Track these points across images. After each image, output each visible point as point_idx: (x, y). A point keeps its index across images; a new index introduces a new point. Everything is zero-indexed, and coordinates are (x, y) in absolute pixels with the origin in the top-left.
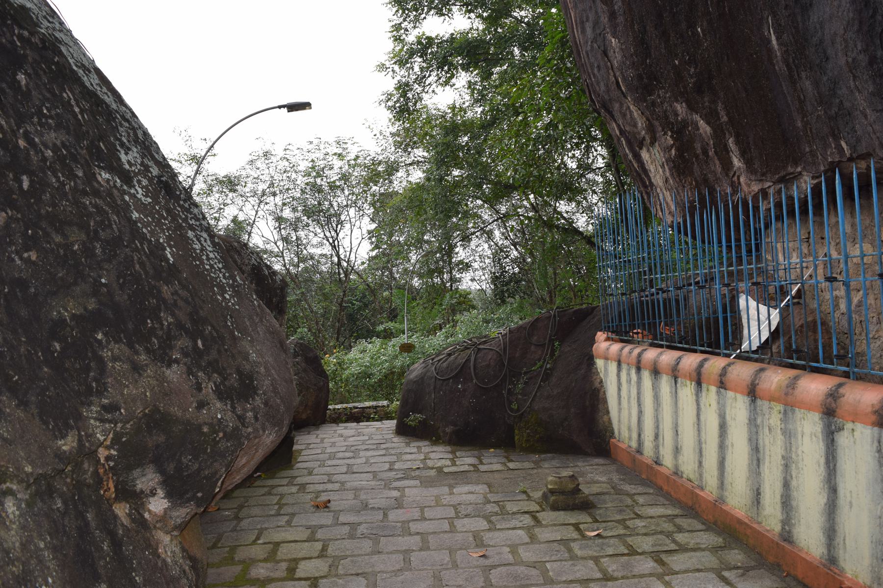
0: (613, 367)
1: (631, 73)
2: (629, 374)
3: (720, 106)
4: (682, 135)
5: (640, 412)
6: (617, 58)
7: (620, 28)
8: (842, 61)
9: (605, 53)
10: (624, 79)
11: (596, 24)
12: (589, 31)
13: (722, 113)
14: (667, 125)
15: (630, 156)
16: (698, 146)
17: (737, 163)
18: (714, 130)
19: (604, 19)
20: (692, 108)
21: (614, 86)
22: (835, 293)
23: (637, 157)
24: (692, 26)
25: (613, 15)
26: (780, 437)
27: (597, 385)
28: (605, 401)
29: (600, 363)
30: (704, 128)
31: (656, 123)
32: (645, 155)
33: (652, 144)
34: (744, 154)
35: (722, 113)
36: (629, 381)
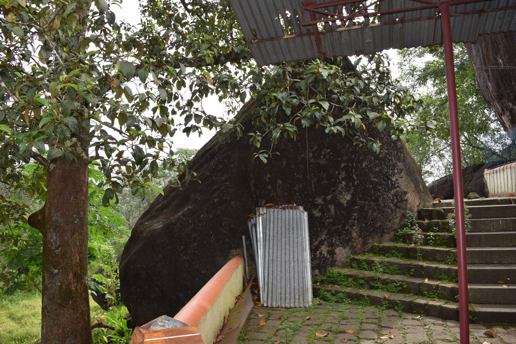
0: (488, 175)
1: (495, 94)
6: (491, 89)
7: (491, 80)
9: (487, 87)
11: (484, 78)
12: (482, 80)
14: (508, 109)
19: (486, 77)
21: (490, 98)
22: (379, 115)
24: (511, 82)
25: (489, 76)
28: (487, 185)
29: (485, 176)
32: (503, 118)
33: (504, 115)
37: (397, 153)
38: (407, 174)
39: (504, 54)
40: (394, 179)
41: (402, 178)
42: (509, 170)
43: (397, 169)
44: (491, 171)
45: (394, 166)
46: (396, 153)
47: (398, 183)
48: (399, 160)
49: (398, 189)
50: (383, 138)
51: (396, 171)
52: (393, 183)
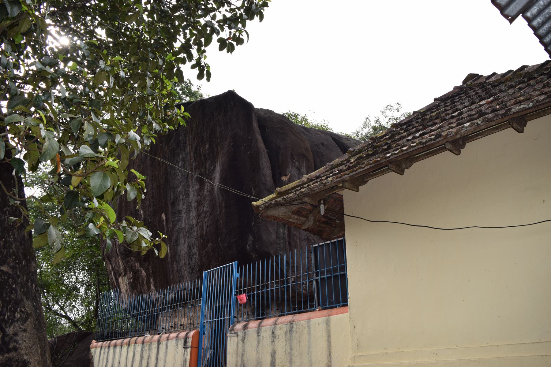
0: (98, 350)
2: (105, 350)
3: (150, 267)
4: (136, 274)
5: (107, 362)
8: (183, 262)
10: (119, 250)
13: (150, 270)
14: (132, 270)
15: (114, 279)
16: (141, 279)
17: (152, 287)
18: (147, 275)
20: (141, 266)
21: (115, 251)
23: (117, 280)
26: (148, 351)
27: (90, 357)
28: (93, 363)
29: (93, 350)
30: (144, 273)
31: (128, 269)
32: (120, 280)
33: (124, 276)
34: (155, 285)
35: (150, 270)
36: (104, 353)
37: (27, 280)
38: (35, 325)
39: (149, 206)
40: (10, 330)
41: (25, 331)
42: (139, 347)
43: (21, 311)
44: (106, 343)
45: (17, 303)
46: (25, 279)
47: (16, 341)
48: (26, 294)
49: (12, 354)
50: (12, 244)
51: (18, 315)
52: (7, 339)
